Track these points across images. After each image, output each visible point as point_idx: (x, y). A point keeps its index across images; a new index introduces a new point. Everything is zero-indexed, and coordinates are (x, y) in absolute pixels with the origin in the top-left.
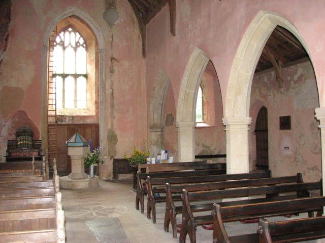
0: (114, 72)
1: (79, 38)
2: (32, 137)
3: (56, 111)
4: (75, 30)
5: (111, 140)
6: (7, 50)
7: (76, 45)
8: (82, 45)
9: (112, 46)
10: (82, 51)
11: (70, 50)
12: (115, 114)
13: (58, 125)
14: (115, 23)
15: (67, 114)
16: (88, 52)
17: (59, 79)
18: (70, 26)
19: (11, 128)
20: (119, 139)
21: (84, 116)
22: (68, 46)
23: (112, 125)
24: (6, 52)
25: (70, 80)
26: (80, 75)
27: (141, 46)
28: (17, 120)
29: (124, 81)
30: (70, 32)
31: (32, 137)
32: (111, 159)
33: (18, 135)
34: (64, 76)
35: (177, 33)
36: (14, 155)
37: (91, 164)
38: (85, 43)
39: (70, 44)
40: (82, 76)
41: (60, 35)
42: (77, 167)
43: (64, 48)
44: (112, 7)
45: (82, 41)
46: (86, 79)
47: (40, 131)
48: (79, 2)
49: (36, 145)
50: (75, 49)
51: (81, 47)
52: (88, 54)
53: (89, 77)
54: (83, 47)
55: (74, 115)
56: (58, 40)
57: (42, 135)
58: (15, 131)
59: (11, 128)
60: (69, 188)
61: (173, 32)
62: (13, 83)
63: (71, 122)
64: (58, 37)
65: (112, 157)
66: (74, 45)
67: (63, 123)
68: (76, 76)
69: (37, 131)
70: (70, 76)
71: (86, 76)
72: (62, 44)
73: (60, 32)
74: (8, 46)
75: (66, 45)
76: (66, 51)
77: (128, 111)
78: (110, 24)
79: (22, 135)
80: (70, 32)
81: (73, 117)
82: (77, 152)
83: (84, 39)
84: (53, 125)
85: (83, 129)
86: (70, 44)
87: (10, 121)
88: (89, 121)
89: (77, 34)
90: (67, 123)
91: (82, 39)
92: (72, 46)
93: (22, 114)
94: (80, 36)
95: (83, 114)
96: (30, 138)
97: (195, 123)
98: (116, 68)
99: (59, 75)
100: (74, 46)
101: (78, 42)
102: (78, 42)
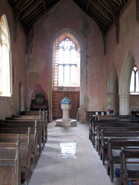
0: (88, 64)
1: (73, 44)
2: (44, 98)
3: (58, 84)
4: (70, 40)
5: (86, 101)
6: (32, 53)
7: (71, 48)
8: (74, 48)
9: (87, 49)
10: (74, 51)
11: (67, 51)
12: (88, 87)
13: (59, 92)
14: (89, 36)
15: (65, 86)
16: (77, 52)
17: (61, 67)
18: (67, 37)
19: (33, 93)
20: (90, 100)
21: (74, 87)
22: (66, 49)
23: (86, 93)
24: (31, 54)
25: (67, 67)
26: (73, 65)
27: (103, 49)
28: (36, 89)
29: (93, 69)
30: (67, 41)
31: (44, 98)
32: (85, 111)
33: (36, 97)
34: (64, 65)
35: (120, 42)
36: (34, 107)
37: (73, 114)
38: (75, 47)
39: (67, 48)
40: (73, 65)
41: (62, 42)
42: (65, 114)
43: (64, 50)
44: (87, 27)
45: (74, 46)
46: (76, 67)
47: (48, 96)
48: (69, 26)
49: (46, 102)
50: (70, 50)
51: (73, 49)
52: (77, 53)
53: (77, 65)
54: (75, 49)
55: (69, 86)
56: (61, 45)
57: (50, 98)
58: (35, 95)
59: (33, 93)
60: (61, 126)
61: (118, 41)
62: (35, 70)
63: (67, 91)
64: (61, 44)
65: (86, 110)
66: (69, 48)
67: (62, 91)
68: (70, 65)
69: (47, 95)
70: (61, 65)
71: (76, 65)
72: (63, 47)
73: (62, 41)
74: (33, 51)
75: (65, 48)
76: (65, 51)
77: (95, 85)
78: (86, 37)
79: (38, 97)
80: (67, 41)
81: (68, 88)
82: (65, 107)
83: (75, 44)
84: (57, 92)
85: (72, 95)
86: (67, 48)
87: (33, 89)
88: (77, 90)
89: (71, 42)
90: (65, 91)
91: (74, 44)
92: (68, 49)
93: (39, 86)
94: (72, 43)
95: (73, 86)
96: (43, 99)
97: (129, 93)
98: (89, 61)
99: (62, 65)
100: (69, 48)
101: (72, 47)
102: (72, 47)
